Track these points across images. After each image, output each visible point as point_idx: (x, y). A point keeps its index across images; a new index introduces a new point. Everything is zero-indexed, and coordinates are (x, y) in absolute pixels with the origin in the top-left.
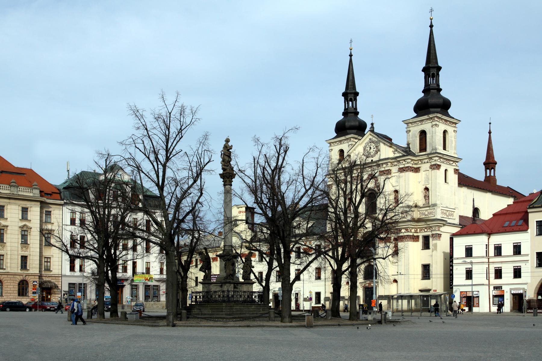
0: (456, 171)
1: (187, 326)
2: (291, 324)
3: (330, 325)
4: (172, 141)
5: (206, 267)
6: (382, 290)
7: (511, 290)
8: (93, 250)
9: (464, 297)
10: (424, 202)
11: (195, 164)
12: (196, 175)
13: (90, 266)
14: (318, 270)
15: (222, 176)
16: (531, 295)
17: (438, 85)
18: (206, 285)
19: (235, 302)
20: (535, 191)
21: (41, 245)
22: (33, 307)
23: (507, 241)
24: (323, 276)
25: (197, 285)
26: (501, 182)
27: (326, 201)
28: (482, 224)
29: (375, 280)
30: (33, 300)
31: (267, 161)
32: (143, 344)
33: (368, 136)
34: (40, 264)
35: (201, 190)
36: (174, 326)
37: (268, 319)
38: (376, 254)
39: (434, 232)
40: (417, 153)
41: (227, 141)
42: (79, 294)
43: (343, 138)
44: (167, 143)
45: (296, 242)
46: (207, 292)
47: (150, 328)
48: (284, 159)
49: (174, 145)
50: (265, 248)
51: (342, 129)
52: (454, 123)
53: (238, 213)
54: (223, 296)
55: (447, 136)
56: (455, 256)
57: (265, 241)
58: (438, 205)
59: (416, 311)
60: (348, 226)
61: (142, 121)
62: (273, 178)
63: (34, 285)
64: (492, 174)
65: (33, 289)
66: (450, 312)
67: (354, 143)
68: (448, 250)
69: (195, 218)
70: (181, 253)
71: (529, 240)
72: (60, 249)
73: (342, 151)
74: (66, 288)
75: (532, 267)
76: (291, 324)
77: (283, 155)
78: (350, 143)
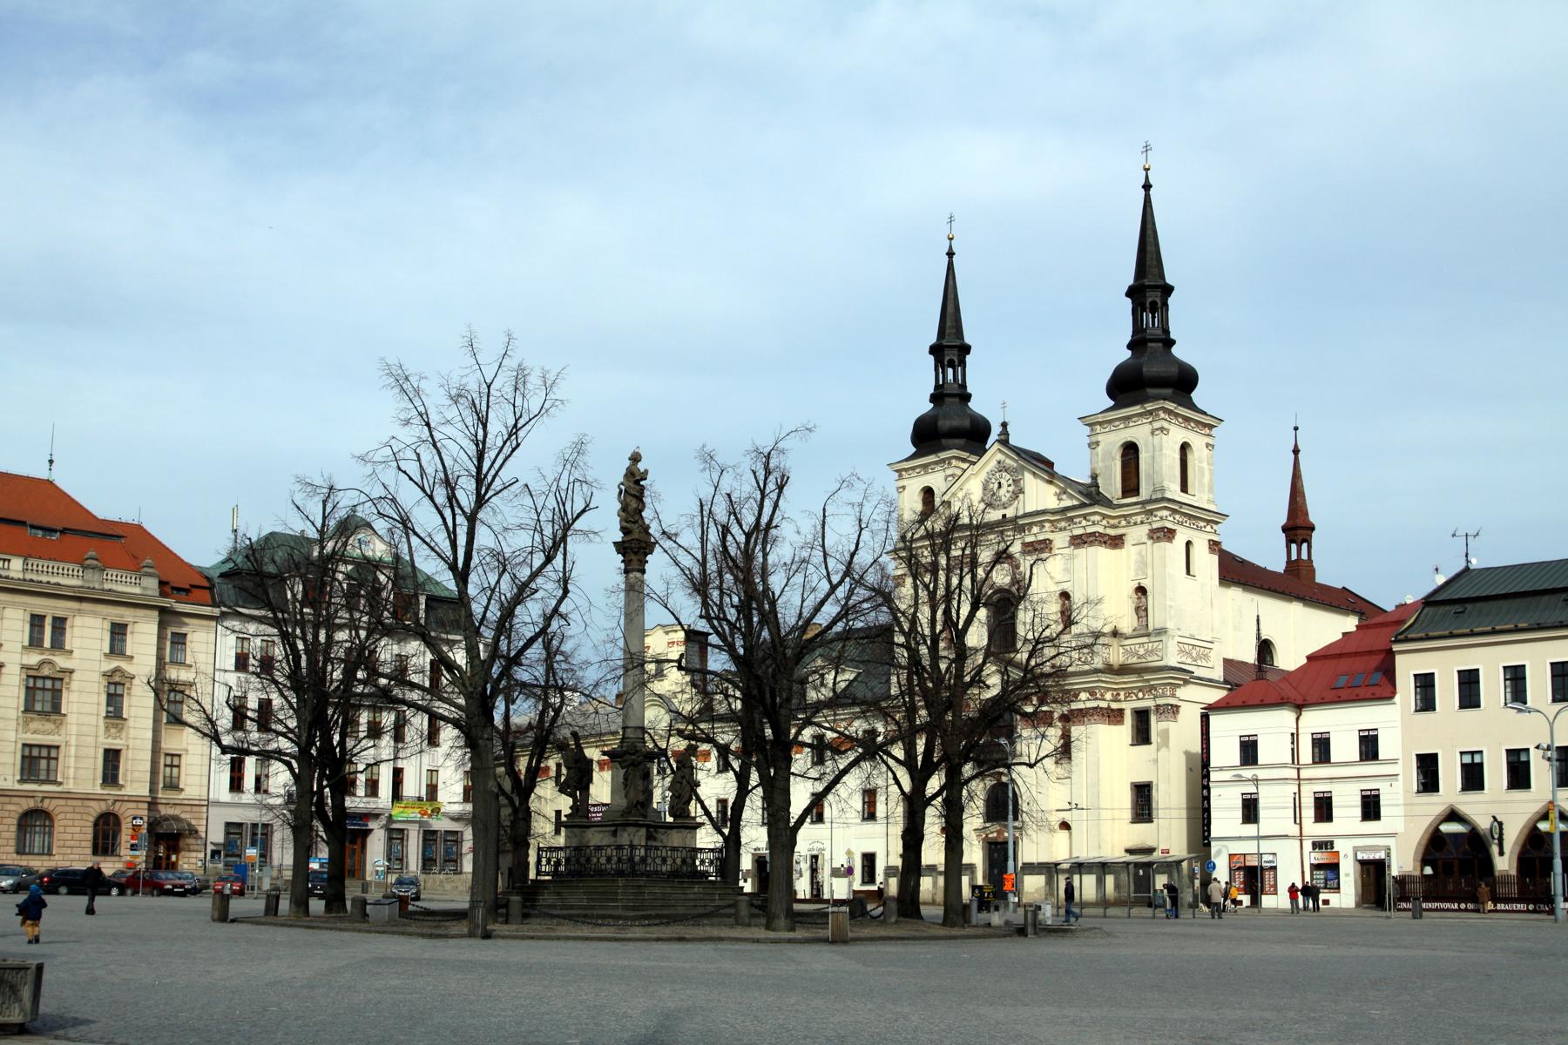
0: (1214, 546)
1: (523, 938)
2: (791, 935)
3: (891, 938)
4: (493, 454)
5: (577, 780)
6: (1033, 848)
7: (1356, 850)
8: (284, 735)
9: (1239, 869)
10: (1135, 624)
11: (550, 515)
12: (549, 543)
13: (281, 778)
14: (870, 795)
15: (621, 547)
16: (1403, 862)
17: (1166, 331)
18: (576, 830)
19: (648, 874)
20: (1409, 600)
21: (156, 721)
22: (129, 884)
23: (1343, 724)
24: (881, 810)
25: (557, 832)
26: (1326, 574)
27: (884, 617)
28: (1281, 681)
29: (1011, 823)
30: (130, 865)
31: (733, 512)
32: (395, 982)
33: (994, 455)
34: (154, 772)
35: (565, 582)
36: (487, 936)
37: (732, 920)
38: (1015, 756)
39: (1161, 701)
40: (1116, 500)
41: (635, 458)
42: (252, 852)
43: (932, 458)
44: (480, 457)
45: (808, 722)
46: (577, 849)
47: (425, 941)
48: (776, 506)
49: (496, 466)
50: (728, 736)
51: (928, 437)
52: (1207, 424)
53: (663, 643)
54: (619, 860)
55: (1190, 457)
56: (1215, 761)
57: (730, 717)
58: (1170, 632)
59: (1118, 903)
60: (938, 677)
61: (418, 403)
62: (748, 555)
63: (136, 828)
64: (1304, 556)
65: (133, 838)
66: (1205, 909)
67: (959, 472)
68: (1197, 748)
69: (550, 654)
70: (514, 746)
71: (1399, 724)
72: (197, 729)
73: (928, 492)
74: (217, 835)
75: (1406, 792)
76: (791, 935)
77: (774, 496)
78: (949, 472)
